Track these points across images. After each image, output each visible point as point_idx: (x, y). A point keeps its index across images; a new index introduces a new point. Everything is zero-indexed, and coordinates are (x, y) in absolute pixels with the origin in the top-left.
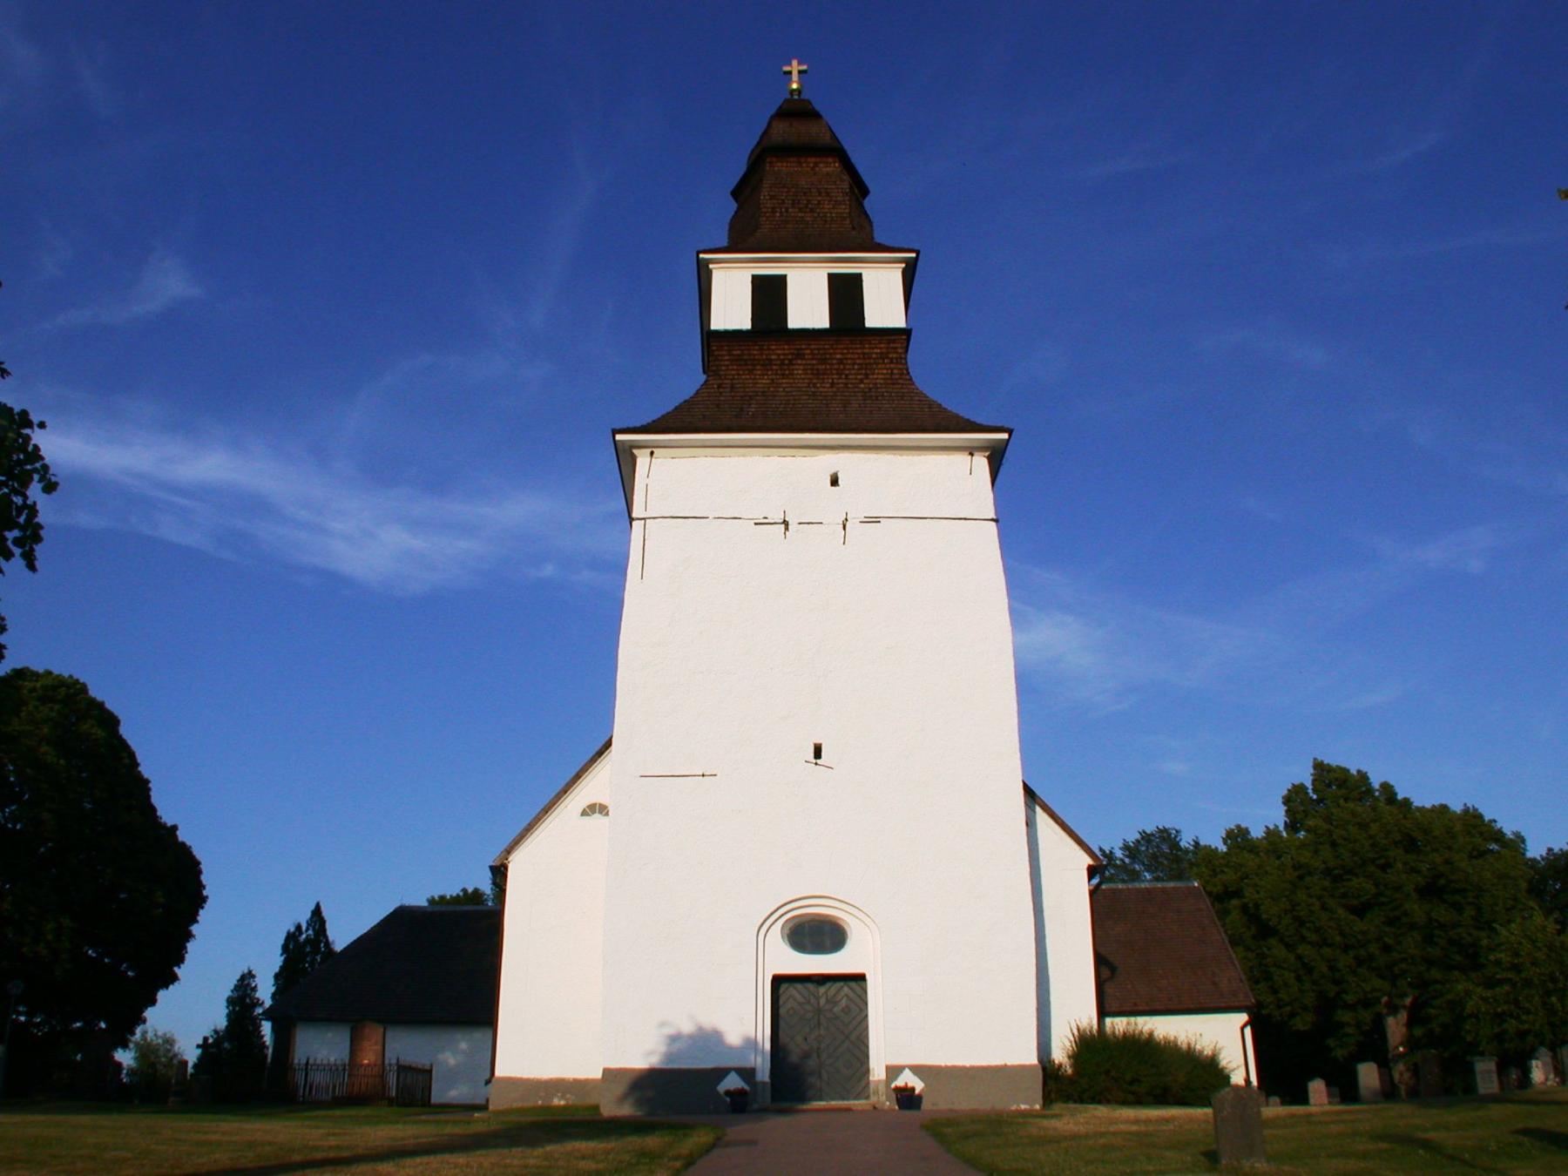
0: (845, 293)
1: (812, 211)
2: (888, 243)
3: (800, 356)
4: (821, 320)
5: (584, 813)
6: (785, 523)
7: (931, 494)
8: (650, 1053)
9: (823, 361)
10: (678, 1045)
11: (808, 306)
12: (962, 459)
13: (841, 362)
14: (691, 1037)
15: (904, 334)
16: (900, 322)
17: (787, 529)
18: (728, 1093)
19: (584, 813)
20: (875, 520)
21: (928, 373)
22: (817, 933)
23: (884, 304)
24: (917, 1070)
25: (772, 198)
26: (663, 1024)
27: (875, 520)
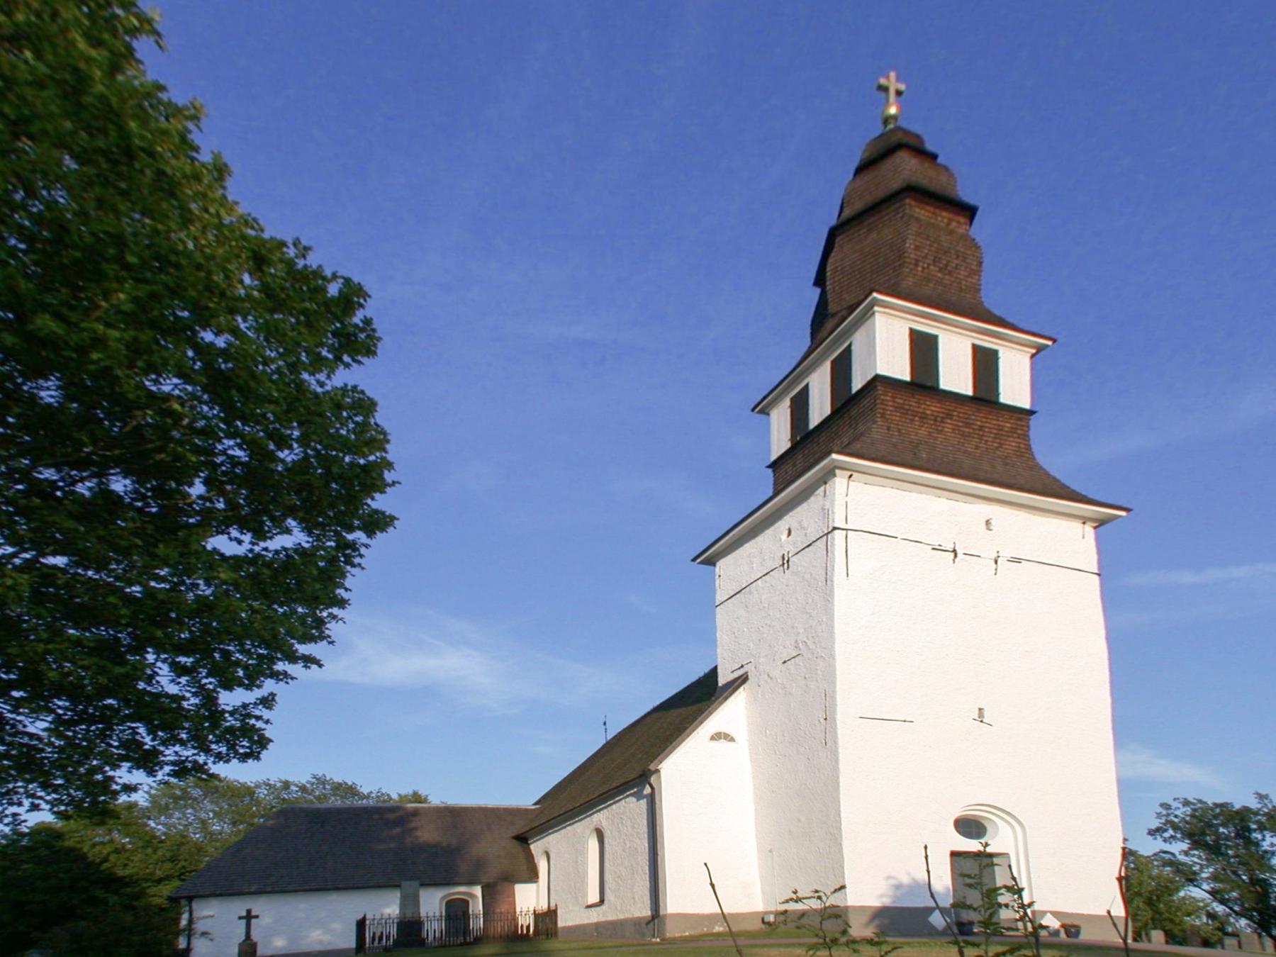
0: (985, 364)
1: (950, 273)
2: (1021, 326)
3: (949, 416)
4: (967, 388)
5: (712, 738)
6: (954, 551)
7: (1050, 550)
8: (882, 896)
9: (968, 425)
10: (899, 893)
11: (956, 374)
12: (1076, 526)
13: (981, 428)
14: (909, 886)
15: (1031, 412)
16: (1026, 404)
17: (956, 556)
18: (310, 533)
19: (712, 738)
20: (1018, 561)
21: (1049, 451)
22: (970, 826)
23: (1015, 386)
24: (1056, 914)
25: (917, 248)
26: (889, 877)
27: (1018, 561)
